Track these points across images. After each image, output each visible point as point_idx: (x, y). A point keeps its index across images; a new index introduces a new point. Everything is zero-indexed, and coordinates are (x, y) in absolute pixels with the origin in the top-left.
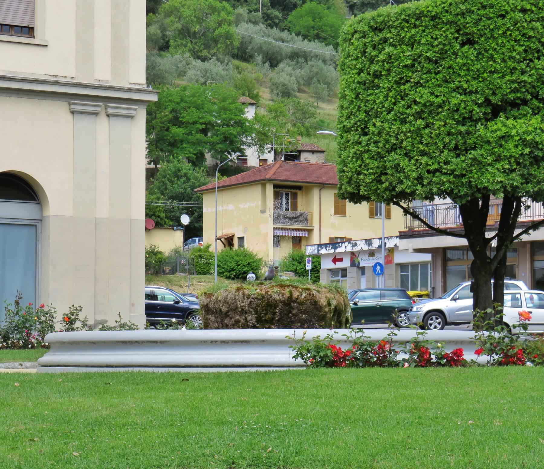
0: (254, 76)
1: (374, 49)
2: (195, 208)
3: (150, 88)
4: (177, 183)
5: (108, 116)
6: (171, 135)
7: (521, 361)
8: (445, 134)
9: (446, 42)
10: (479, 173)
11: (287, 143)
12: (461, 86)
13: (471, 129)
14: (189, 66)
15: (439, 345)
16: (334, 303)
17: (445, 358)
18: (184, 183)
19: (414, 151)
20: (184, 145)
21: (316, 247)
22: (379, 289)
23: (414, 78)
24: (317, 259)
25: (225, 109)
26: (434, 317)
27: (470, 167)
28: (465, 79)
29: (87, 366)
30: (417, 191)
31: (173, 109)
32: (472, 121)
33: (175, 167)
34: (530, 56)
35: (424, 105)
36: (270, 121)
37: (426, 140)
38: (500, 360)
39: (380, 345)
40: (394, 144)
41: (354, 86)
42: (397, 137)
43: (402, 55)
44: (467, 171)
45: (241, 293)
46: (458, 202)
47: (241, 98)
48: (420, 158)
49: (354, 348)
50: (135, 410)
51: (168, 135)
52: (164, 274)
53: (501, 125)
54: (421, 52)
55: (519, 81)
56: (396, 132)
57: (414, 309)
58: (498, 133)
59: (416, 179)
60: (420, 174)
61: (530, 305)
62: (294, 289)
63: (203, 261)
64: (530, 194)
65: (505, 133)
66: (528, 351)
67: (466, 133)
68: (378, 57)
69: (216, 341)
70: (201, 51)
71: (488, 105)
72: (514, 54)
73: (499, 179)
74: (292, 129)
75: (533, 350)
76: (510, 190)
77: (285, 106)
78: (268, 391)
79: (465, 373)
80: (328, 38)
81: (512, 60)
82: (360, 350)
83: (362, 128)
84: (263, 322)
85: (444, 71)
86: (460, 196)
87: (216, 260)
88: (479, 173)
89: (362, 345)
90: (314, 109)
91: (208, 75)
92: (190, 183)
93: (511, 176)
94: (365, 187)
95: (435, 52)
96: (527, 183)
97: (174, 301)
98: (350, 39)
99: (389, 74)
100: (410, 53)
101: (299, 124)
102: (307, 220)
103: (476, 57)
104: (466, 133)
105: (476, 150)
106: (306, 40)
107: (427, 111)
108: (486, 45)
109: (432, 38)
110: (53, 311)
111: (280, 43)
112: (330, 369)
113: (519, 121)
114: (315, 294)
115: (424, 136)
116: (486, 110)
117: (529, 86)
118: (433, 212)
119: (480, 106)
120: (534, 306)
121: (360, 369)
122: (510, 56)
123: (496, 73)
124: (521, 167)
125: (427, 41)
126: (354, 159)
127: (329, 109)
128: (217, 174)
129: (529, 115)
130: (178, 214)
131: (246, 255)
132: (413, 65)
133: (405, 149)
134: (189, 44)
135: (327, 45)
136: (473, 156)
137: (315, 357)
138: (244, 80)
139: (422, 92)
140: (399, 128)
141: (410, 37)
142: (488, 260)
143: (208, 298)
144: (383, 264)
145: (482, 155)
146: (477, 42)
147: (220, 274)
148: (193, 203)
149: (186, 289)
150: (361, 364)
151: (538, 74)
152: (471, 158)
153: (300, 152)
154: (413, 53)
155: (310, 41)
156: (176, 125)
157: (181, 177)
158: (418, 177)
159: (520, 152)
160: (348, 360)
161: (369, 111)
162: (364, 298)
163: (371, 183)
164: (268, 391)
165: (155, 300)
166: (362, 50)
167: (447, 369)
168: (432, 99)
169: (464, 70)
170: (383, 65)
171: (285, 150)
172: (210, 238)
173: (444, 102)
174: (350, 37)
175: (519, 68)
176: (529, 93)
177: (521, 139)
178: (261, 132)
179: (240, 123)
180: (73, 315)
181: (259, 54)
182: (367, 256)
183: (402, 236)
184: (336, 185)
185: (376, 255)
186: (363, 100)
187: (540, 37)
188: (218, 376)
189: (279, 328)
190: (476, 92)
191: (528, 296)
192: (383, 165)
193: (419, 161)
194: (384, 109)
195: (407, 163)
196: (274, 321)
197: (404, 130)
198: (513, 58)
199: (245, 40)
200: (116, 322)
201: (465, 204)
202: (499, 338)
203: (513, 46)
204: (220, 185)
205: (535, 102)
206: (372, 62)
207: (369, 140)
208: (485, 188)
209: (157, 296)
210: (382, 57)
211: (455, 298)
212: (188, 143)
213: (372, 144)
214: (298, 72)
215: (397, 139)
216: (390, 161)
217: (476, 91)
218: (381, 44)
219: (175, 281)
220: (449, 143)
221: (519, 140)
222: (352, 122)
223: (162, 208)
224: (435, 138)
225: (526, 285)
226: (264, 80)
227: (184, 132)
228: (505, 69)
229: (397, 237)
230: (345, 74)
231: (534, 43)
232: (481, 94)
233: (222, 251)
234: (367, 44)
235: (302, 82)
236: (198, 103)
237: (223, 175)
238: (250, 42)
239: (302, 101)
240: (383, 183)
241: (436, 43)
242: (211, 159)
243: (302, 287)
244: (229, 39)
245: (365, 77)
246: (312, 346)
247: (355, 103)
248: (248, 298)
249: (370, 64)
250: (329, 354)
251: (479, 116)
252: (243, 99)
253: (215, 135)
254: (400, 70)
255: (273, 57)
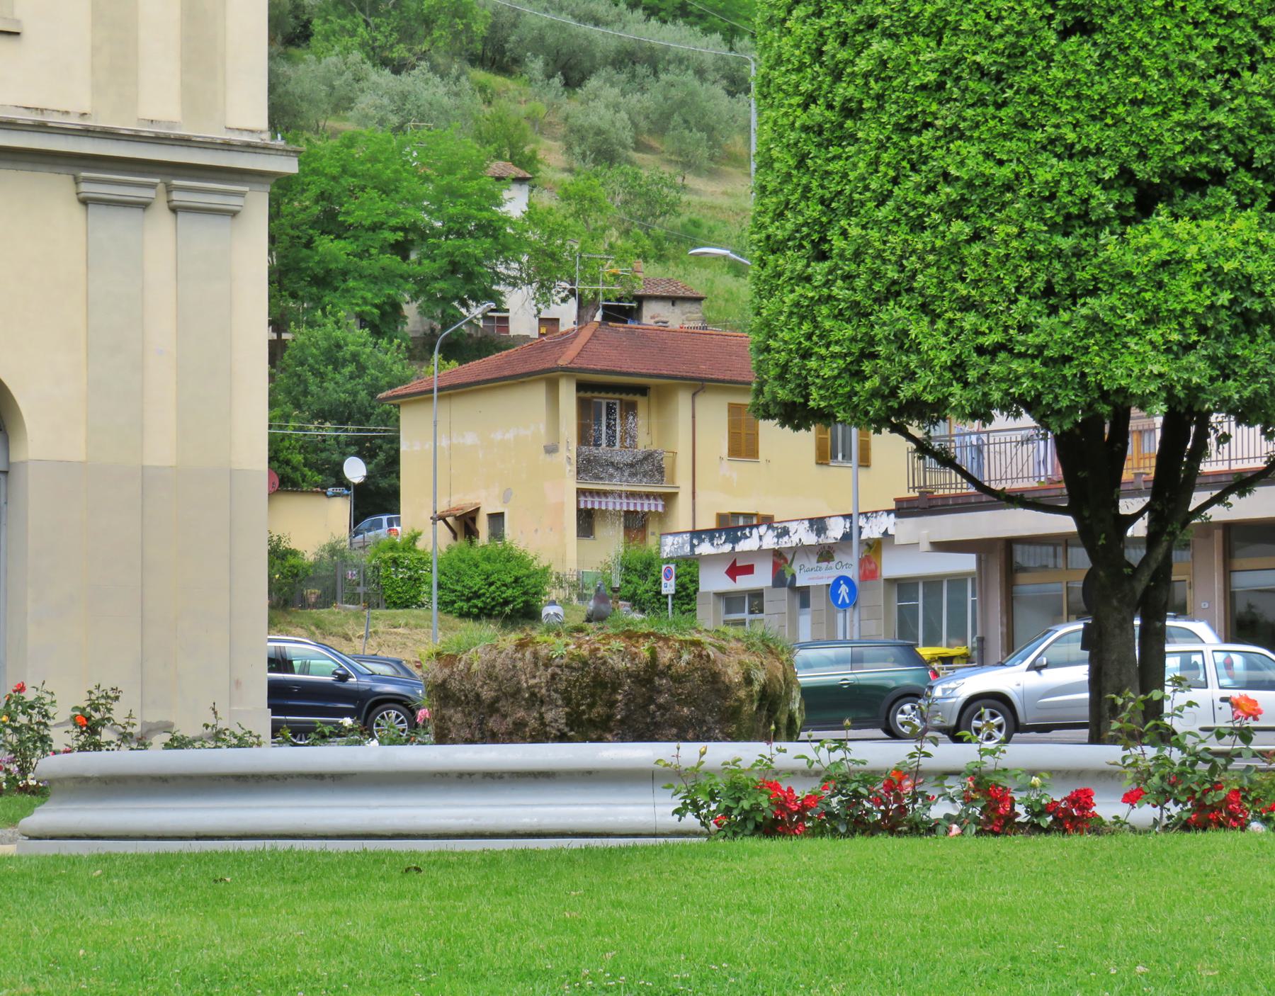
0: (524, 109)
1: (843, 44)
2: (379, 441)
3: (279, 142)
4: (333, 379)
5: (174, 210)
6: (317, 258)
7: (1236, 819)
8: (1022, 257)
9: (1024, 28)
10: (1105, 354)
11: (613, 276)
12: (1061, 138)
13: (1084, 244)
14: (363, 84)
15: (1035, 780)
16: (760, 677)
17: (1050, 814)
18: (351, 378)
19: (943, 299)
20: (351, 284)
21: (687, 537)
22: (844, 642)
23: (944, 118)
24: (689, 565)
25: (453, 193)
26: (986, 712)
27: (1082, 339)
28: (1070, 119)
29: (145, 838)
30: (951, 399)
31: (322, 193)
32: (1089, 223)
33: (328, 337)
34: (1233, 63)
35: (970, 185)
36: (566, 223)
37: (973, 270)
38: (1185, 816)
39: (890, 781)
40: (894, 282)
41: (793, 136)
42: (902, 265)
43: (912, 59)
44: (1075, 349)
45: (528, 655)
46: (1055, 427)
47: (493, 165)
48: (959, 315)
49: (825, 788)
50: (307, 943)
51: (310, 257)
52: (303, 607)
53: (1160, 233)
54: (960, 51)
55: (1205, 124)
56: (899, 252)
57: (938, 692)
58: (1154, 253)
59: (950, 369)
60: (958, 357)
61: (1226, 681)
62: (661, 644)
63: (402, 574)
64: (1231, 405)
65: (1169, 254)
66: (1253, 794)
67: (1074, 255)
68: (854, 65)
69: (471, 774)
70: (392, 46)
71: (1127, 185)
72: (1192, 57)
73: (1156, 369)
74: (619, 242)
75: (1268, 792)
76: (1182, 395)
77: (603, 184)
78: (625, 896)
79: (1103, 849)
80: (708, 15)
81: (1188, 73)
82: (840, 792)
83: (813, 241)
84: (583, 727)
85: (1018, 99)
86: (1059, 411)
87: (435, 570)
88: (1105, 354)
89: (846, 780)
90: (674, 193)
91: (408, 106)
92: (367, 379)
93: (1184, 362)
94: (821, 388)
95: (995, 52)
96: (1227, 377)
97: (334, 673)
98: (784, 20)
99: (881, 107)
100: (934, 56)
101: (637, 230)
102: (660, 470)
103: (1098, 65)
104: (1074, 255)
105: (1099, 297)
106: (653, 21)
107: (977, 199)
108: (1122, 34)
109: (988, 16)
110: (48, 699)
111: (589, 27)
112: (767, 842)
113: (1204, 223)
114: (712, 656)
115: (969, 260)
116: (1122, 196)
117: (1228, 136)
118: (979, 450)
119: (1107, 186)
120: (1235, 683)
121: (843, 842)
122: (1181, 62)
123: (1148, 104)
124: (1208, 338)
125: (976, 24)
126: (795, 320)
127: (713, 193)
128: (436, 356)
129: (1229, 210)
130: (336, 457)
131: (510, 557)
132: (941, 86)
133: (921, 295)
134: (360, 30)
135: (707, 31)
136: (1090, 312)
137: (728, 810)
138: (500, 120)
139: (964, 152)
140: (906, 241)
141: (934, 15)
142: (1127, 571)
143: (446, 666)
144: (856, 580)
145: (1112, 309)
146: (1101, 28)
147: (445, 605)
148: (374, 429)
149: (358, 646)
150: (842, 829)
151: (1251, 108)
152: (1085, 317)
153: (640, 299)
154: (940, 54)
155: (665, 22)
156: (329, 233)
157: (344, 363)
158: (954, 363)
159: (1208, 302)
160: (811, 819)
161: (832, 200)
162: (808, 665)
163: (836, 378)
164: (625, 896)
165: (286, 672)
166: (814, 46)
167: (1055, 839)
168: (989, 168)
169: (1068, 98)
170: (866, 84)
171: (604, 294)
172: (418, 518)
173: (1017, 175)
174: (782, 15)
175: (1205, 92)
176: (1229, 155)
177: (1209, 268)
178: (544, 251)
179: (490, 229)
180: (97, 710)
181: (536, 56)
182: (814, 559)
183: (904, 509)
184: (749, 383)
185: (837, 558)
186: (815, 171)
187: (1255, 14)
188: (492, 861)
189: (623, 740)
190: (1099, 152)
191: (1220, 658)
192: (866, 333)
193: (957, 323)
194: (868, 194)
195: (925, 330)
196: (612, 724)
197: (920, 246)
198: (1190, 67)
199: (502, 20)
200: (207, 726)
201: (1071, 430)
202: (1183, 763)
203: (1189, 37)
204: (444, 384)
205: (1243, 176)
206: (837, 76)
207: (831, 272)
208: (1122, 390)
209: (291, 662)
210: (863, 64)
211: (1038, 663)
212: (361, 277)
213: (839, 283)
214: (634, 99)
215: (902, 269)
216: (884, 324)
217: (1098, 149)
218: (861, 31)
219: (331, 623)
220: (1031, 278)
221: (1205, 271)
222: (789, 226)
223: (297, 440)
224: (997, 266)
225: (1213, 629)
226: (547, 119)
227: (349, 249)
228: (1170, 96)
229: (889, 512)
230: (771, 106)
231: (1243, 30)
232: (1111, 158)
233: (450, 549)
234: (826, 33)
235: (644, 124)
236: (385, 177)
237: (447, 358)
238: (514, 25)
239: (644, 173)
240: (866, 378)
241: (998, 29)
242: (418, 318)
243: (681, 638)
244: (461, 18)
245: (822, 115)
246: (721, 784)
247: (795, 180)
248: (546, 666)
249: (834, 82)
250: (765, 805)
251: (1106, 213)
252: (497, 167)
253: (428, 257)
254: (907, 96)
255: (573, 62)
